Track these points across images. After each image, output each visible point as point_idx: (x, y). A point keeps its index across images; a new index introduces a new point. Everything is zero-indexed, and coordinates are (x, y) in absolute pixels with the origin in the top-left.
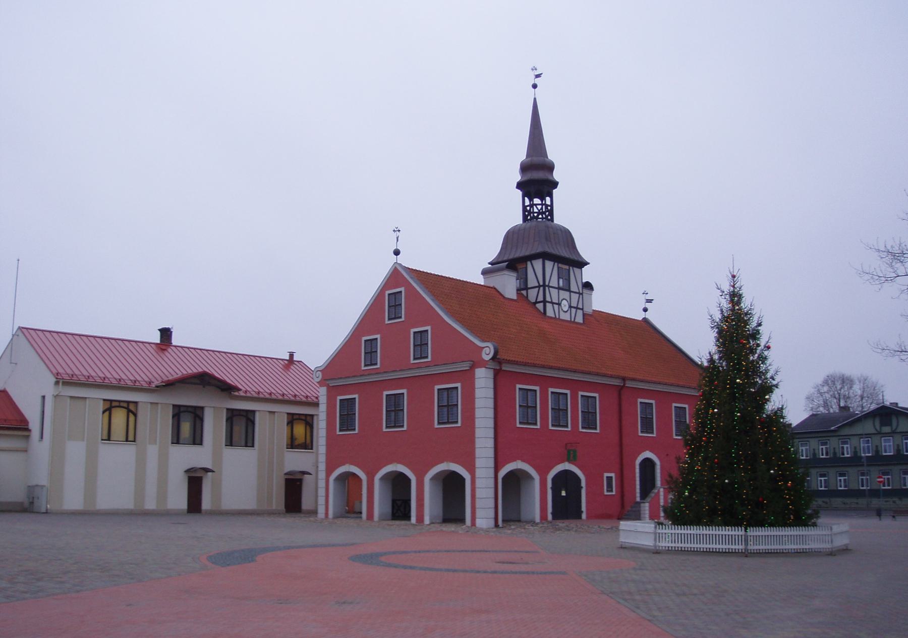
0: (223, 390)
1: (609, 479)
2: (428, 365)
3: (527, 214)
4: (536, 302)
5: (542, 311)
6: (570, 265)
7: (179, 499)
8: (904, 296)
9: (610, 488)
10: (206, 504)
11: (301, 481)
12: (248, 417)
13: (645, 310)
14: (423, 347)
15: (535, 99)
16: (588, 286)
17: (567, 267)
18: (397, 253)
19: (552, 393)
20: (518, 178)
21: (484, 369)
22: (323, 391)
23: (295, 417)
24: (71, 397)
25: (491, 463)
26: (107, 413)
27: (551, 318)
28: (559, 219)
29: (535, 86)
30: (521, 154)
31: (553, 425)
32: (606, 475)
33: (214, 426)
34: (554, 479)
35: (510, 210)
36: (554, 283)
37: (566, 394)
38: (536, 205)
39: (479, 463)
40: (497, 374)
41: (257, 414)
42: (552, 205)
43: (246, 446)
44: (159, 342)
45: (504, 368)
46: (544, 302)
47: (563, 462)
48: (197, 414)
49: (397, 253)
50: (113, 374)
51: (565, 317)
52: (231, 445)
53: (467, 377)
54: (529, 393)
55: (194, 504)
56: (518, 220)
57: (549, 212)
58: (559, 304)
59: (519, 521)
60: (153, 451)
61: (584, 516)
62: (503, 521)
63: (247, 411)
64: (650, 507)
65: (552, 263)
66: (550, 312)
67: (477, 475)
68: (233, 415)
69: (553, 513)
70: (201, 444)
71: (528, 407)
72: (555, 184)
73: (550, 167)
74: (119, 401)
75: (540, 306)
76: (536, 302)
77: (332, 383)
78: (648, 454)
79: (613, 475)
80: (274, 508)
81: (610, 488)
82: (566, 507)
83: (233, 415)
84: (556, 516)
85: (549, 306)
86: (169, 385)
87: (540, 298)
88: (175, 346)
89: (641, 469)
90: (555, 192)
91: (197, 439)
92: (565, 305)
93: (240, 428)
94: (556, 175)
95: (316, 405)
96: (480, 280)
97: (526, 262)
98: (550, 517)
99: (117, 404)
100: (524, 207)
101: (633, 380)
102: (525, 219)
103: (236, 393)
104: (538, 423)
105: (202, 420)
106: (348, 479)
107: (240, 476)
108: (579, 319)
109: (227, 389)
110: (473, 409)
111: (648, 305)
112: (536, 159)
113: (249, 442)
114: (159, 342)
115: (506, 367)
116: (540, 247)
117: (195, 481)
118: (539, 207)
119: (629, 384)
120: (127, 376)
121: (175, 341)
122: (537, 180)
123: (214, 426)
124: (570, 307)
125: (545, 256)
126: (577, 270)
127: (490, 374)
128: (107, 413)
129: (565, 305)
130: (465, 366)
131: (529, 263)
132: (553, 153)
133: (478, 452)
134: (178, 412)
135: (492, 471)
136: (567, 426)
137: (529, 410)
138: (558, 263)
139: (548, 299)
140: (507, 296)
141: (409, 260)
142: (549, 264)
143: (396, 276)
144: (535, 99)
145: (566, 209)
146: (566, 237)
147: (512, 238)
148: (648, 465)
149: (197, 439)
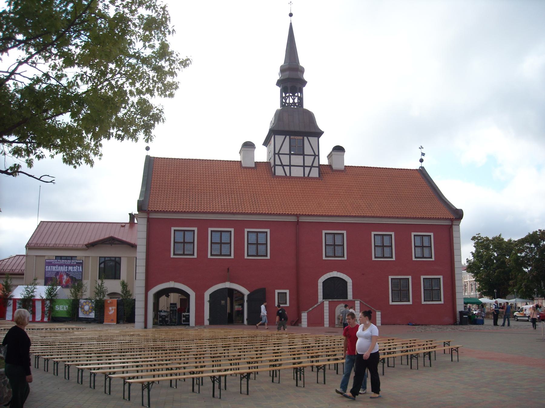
13: (421, 161)
15: (291, 24)
17: (301, 138)
23: (106, 259)
25: (143, 283)
28: (306, 106)
30: (280, 59)
34: (211, 295)
35: (271, 101)
50: (61, 242)
65: (284, 136)
69: (209, 320)
72: (304, 83)
73: (302, 70)
74: (110, 257)
86: (92, 246)
89: (210, 302)
90: (305, 89)
94: (306, 77)
98: (207, 322)
99: (109, 259)
105: (120, 264)
108: (315, 173)
116: (295, 126)
119: (302, 219)
120: (71, 242)
122: (292, 80)
126: (313, 140)
131: (305, 138)
132: (303, 62)
135: (143, 290)
138: (290, 136)
144: (291, 24)
145: (312, 99)
146: (309, 117)
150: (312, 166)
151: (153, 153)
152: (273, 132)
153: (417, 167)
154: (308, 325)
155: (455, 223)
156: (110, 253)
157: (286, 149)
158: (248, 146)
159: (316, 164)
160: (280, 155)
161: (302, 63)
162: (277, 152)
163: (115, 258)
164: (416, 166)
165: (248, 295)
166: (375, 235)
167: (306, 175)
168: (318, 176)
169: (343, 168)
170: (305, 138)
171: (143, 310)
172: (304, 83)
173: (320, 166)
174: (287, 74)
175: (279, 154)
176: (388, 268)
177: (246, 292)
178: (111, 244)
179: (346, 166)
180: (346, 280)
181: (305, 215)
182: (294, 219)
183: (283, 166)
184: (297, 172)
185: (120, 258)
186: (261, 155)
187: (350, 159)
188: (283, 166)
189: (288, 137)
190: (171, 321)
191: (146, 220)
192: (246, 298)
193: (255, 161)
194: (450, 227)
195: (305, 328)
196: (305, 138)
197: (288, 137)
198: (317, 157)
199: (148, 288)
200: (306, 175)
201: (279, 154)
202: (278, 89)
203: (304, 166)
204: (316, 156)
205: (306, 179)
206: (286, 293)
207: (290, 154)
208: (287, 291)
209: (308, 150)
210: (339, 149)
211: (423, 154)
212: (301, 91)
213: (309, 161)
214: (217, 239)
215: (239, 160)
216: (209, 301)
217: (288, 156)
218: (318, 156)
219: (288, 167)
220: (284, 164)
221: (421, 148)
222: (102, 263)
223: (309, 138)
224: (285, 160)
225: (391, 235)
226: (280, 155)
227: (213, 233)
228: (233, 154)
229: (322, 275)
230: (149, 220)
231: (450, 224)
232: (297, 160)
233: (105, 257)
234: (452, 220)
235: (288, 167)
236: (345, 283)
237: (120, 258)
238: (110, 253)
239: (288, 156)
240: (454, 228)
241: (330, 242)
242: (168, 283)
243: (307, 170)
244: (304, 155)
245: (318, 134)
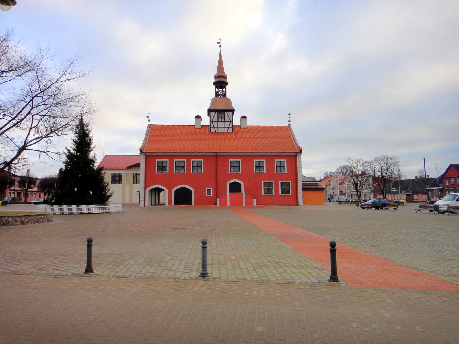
1: (209, 191)
3: (217, 95)
8: (3, 35)
15: (220, 51)
18: (289, 121)
20: (213, 80)
28: (228, 96)
30: (215, 72)
34: (175, 191)
38: (220, 91)
42: (226, 92)
49: (289, 121)
56: (214, 96)
57: (224, 95)
60: (127, 187)
61: (193, 203)
65: (215, 112)
69: (175, 202)
72: (227, 84)
81: (209, 191)
82: (183, 198)
84: (176, 203)
90: (227, 87)
94: (228, 80)
98: (173, 204)
99: (116, 174)
100: (216, 92)
104: (158, 173)
108: (230, 130)
111: (148, 115)
112: (220, 74)
118: (221, 92)
119: (218, 154)
122: (221, 83)
126: (230, 114)
131: (226, 113)
132: (226, 72)
144: (220, 51)
150: (229, 127)
151: (151, 123)
152: (210, 111)
155: (298, 154)
157: (216, 119)
158: (198, 117)
159: (231, 126)
160: (230, 121)
162: (211, 120)
166: (193, 161)
167: (226, 132)
169: (246, 127)
170: (226, 113)
171: (144, 198)
173: (233, 127)
174: (218, 80)
175: (212, 121)
176: (263, 177)
180: (240, 183)
181: (220, 152)
184: (221, 130)
186: (206, 121)
187: (250, 122)
191: (144, 156)
193: (202, 125)
194: (296, 156)
197: (217, 113)
198: (232, 122)
199: (145, 188)
200: (226, 132)
201: (212, 121)
202: (214, 87)
203: (225, 127)
204: (231, 121)
205: (226, 133)
206: (211, 190)
207: (218, 121)
208: (212, 189)
209: (227, 119)
210: (244, 117)
212: (225, 87)
213: (227, 124)
214: (195, 165)
215: (194, 125)
217: (217, 122)
218: (232, 121)
221: (290, 114)
222: (135, 176)
223: (4, 133)
224: (216, 124)
225: (285, 161)
226: (230, 121)
227: (176, 162)
228: (192, 122)
229: (230, 180)
230: (145, 156)
231: (295, 155)
232: (221, 124)
233: (136, 173)
234: (296, 153)
236: (240, 185)
239: (217, 122)
240: (298, 157)
241: (195, 165)
243: (227, 129)
244: (225, 121)
245: (233, 111)
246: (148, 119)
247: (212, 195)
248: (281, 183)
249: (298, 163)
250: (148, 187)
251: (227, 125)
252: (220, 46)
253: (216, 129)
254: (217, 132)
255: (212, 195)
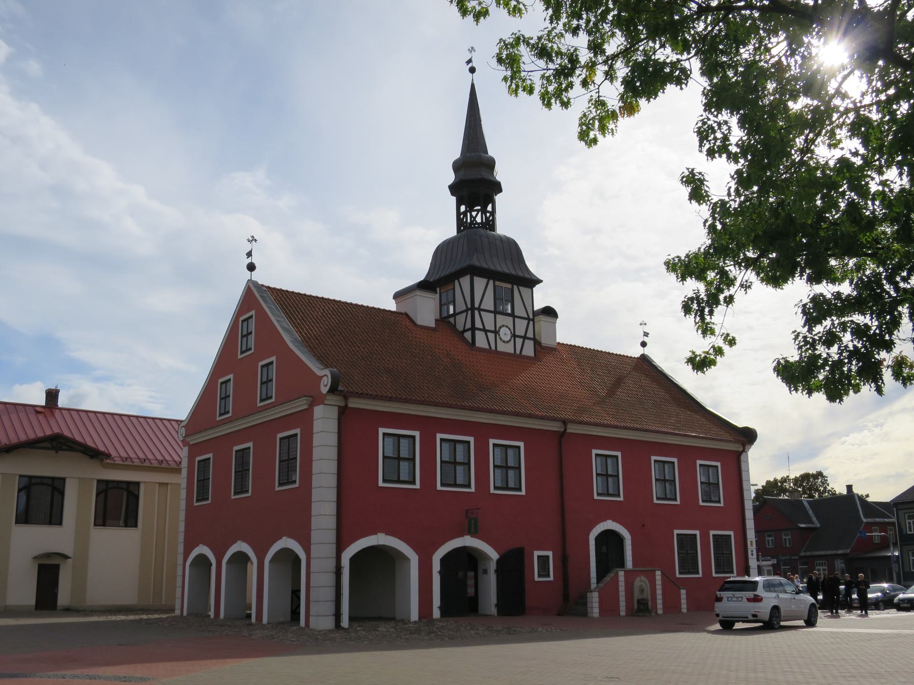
0: (92, 457)
1: (543, 560)
2: (273, 405)
4: (465, 331)
5: (470, 340)
6: (513, 284)
7: (23, 591)
9: (544, 571)
10: (64, 597)
11: (57, 567)
12: (131, 490)
13: (644, 344)
14: (270, 384)
15: (473, 86)
16: (549, 312)
17: (509, 286)
19: (700, 465)
20: (451, 178)
21: (322, 406)
22: (184, 452)
23: (34, 481)
24: (160, 484)
25: (332, 537)
26: (102, 495)
27: (481, 350)
28: (503, 228)
29: (472, 70)
30: (455, 151)
31: (703, 501)
32: (537, 553)
33: (77, 502)
34: (443, 561)
35: (441, 221)
36: (489, 303)
37: (717, 467)
39: (315, 537)
40: (343, 413)
41: (142, 487)
43: (126, 526)
44: (44, 404)
45: (350, 405)
46: (473, 329)
47: (461, 535)
48: (56, 487)
51: (508, 348)
52: (104, 525)
53: (305, 419)
54: (711, 470)
55: (46, 598)
57: (490, 224)
58: (496, 332)
59: (394, 619)
62: (352, 619)
63: (128, 483)
64: (600, 597)
65: (485, 280)
66: (481, 341)
67: (312, 556)
68: (106, 488)
69: (440, 608)
70: (60, 523)
71: (665, 481)
73: (490, 164)
74: (42, 478)
75: (468, 335)
76: (465, 331)
77: (193, 440)
78: (609, 525)
79: (550, 553)
80: (163, 602)
81: (544, 571)
83: (106, 488)
85: (480, 336)
87: (469, 325)
88: (61, 409)
90: (498, 198)
91: (54, 518)
92: (505, 334)
93: (118, 505)
94: (500, 174)
95: (178, 471)
96: (392, 306)
97: (454, 281)
98: (436, 614)
101: (361, 396)
102: (459, 230)
103: (108, 461)
105: (62, 494)
106: (202, 561)
107: (111, 563)
108: (529, 350)
109: (95, 455)
110: (311, 461)
113: (131, 520)
114: (44, 404)
115: (354, 403)
117: (48, 572)
119: (572, 429)
121: (62, 402)
122: (475, 182)
123: (77, 502)
124: (514, 336)
125: (474, 271)
127: (333, 413)
128: (102, 495)
129: (505, 334)
130: (300, 405)
131: (456, 282)
132: (495, 146)
133: (315, 522)
134: (29, 485)
135: (332, 550)
136: (719, 502)
137: (610, 479)
138: (495, 280)
139: (478, 324)
140: (419, 322)
141: (262, 277)
142: (480, 283)
143: (254, 297)
144: (473, 86)
146: (511, 249)
147: (443, 252)
148: (610, 540)
149: (54, 518)
153: (637, 355)
154: (442, 615)
156: (43, 466)
161: (492, 151)
163: (53, 479)
164: (635, 352)
165: (498, 561)
168: (533, 355)
172: (497, 188)
177: (494, 555)
178: (57, 449)
179: (559, 343)
182: (556, 427)
183: (486, 331)
185: (64, 479)
188: (486, 331)
189: (491, 282)
190: (672, 606)
192: (493, 567)
195: (437, 620)
196: (515, 287)
198: (531, 323)
211: (646, 334)
216: (440, 572)
219: (528, 336)
220: (487, 328)
235: (528, 336)
237: (64, 479)
238: (43, 466)
240: (743, 457)
242: (461, 539)
246: (646, 339)
247: (551, 578)
248: (539, 557)
249: (744, 474)
250: (478, 538)
251: (520, 331)
252: (472, 70)
253: (491, 336)
254: (518, 352)
255: (551, 578)
